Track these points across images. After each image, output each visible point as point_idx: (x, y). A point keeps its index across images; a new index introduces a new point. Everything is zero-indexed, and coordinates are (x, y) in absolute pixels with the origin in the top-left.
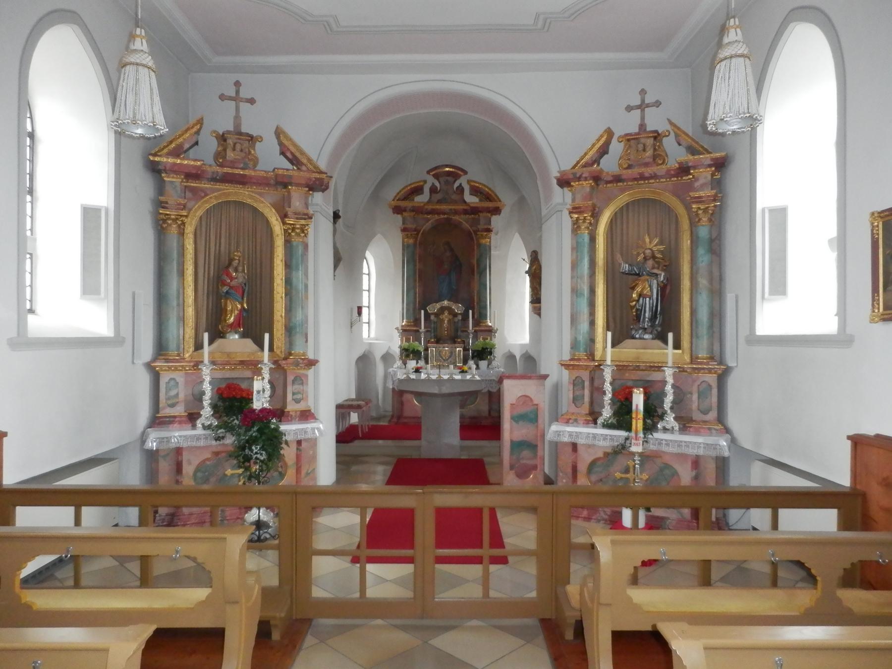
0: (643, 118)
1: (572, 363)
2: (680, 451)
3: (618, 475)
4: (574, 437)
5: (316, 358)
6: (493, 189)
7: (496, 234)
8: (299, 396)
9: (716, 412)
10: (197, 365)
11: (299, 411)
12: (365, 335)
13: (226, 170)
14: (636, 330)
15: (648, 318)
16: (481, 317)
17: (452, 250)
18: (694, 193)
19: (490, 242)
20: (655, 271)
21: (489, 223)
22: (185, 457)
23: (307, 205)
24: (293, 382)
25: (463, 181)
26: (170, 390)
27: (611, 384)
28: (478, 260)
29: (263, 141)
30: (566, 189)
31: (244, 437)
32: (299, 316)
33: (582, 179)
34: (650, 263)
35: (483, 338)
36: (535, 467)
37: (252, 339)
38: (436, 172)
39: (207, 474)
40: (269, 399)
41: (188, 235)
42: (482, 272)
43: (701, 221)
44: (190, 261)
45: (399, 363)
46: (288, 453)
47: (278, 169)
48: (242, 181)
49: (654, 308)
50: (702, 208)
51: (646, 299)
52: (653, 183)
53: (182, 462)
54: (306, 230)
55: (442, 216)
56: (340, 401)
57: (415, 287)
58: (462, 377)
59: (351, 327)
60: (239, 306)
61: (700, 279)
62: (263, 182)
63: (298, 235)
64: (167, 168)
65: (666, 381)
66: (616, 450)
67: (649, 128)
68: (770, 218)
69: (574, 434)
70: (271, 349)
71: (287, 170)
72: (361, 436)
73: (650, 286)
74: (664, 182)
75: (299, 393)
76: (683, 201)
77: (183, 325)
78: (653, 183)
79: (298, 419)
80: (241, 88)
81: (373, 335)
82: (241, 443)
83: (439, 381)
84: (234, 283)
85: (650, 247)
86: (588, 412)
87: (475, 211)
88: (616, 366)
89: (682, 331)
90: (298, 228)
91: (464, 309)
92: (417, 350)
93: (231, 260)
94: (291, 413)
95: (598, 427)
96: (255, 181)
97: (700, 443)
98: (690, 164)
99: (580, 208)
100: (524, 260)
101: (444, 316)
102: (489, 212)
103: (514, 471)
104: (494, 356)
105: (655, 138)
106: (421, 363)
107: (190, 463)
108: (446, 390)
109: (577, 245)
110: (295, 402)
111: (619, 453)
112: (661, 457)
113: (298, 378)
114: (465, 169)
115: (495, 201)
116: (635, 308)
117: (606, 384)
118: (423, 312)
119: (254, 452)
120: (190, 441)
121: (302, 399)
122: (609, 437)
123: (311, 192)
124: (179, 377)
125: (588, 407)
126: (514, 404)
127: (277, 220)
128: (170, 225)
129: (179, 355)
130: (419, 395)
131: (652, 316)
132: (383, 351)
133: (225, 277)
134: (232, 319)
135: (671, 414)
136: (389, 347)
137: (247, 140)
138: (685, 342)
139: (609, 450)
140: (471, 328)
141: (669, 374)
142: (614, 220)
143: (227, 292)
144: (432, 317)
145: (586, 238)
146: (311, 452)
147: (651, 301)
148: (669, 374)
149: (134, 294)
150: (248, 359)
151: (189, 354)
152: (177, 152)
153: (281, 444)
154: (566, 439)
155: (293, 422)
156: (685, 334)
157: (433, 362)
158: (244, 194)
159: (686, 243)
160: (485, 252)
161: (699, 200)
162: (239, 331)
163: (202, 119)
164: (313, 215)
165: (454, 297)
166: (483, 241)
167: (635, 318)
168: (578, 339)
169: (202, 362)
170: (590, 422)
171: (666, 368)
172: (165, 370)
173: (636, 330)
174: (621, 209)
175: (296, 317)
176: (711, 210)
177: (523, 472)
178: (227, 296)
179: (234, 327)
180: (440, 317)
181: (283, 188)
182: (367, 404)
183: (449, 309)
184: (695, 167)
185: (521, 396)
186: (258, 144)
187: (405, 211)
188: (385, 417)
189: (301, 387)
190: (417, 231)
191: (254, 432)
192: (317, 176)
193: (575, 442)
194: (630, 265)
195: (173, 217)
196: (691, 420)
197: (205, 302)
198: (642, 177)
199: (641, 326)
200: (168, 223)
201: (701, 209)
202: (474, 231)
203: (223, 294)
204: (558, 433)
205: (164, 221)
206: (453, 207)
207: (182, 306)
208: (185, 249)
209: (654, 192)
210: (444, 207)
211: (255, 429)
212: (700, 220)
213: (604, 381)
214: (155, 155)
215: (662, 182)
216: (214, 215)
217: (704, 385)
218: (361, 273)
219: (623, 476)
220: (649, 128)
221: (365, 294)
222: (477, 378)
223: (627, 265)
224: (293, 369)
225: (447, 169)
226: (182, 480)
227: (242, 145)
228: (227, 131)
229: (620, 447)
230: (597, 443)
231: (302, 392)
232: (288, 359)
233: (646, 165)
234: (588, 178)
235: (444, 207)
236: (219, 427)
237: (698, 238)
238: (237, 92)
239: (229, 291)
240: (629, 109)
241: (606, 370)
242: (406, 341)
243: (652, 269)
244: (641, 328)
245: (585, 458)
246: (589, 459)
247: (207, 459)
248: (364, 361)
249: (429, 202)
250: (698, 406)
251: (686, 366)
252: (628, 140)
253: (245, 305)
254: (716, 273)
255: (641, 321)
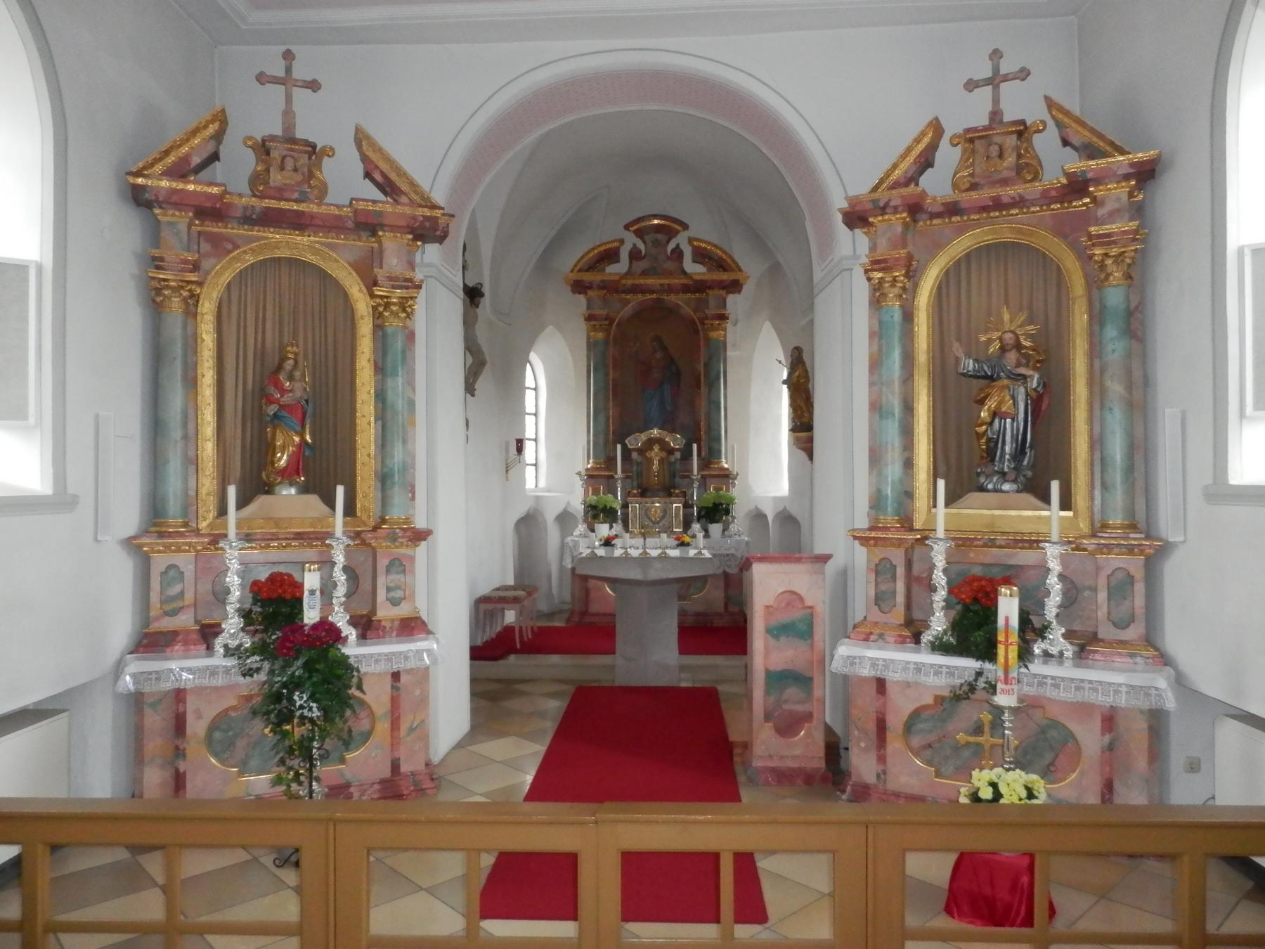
0: (996, 100)
1: (873, 534)
2: (1080, 699)
3: (962, 737)
4: (880, 667)
5: (430, 528)
6: (728, 250)
7: (735, 324)
8: (399, 594)
9: (1144, 624)
10: (217, 538)
11: (397, 619)
12: (530, 483)
13: (268, 203)
14: (987, 477)
15: (1010, 455)
16: (711, 455)
17: (665, 349)
18: (1097, 228)
19: (725, 336)
20: (1022, 371)
21: (724, 305)
22: (191, 705)
23: (412, 265)
24: (388, 571)
25: (681, 240)
26: (169, 585)
27: (945, 571)
28: (706, 365)
29: (336, 154)
30: (857, 231)
31: (279, 679)
32: (398, 455)
33: (888, 210)
34: (1012, 357)
35: (715, 488)
36: (808, 717)
37: (318, 495)
38: (638, 227)
39: (230, 733)
40: (344, 599)
41: (205, 316)
42: (713, 384)
43: (1111, 278)
44: (208, 361)
45: (581, 528)
46: (375, 695)
47: (357, 200)
48: (299, 223)
49: (1020, 437)
50: (1112, 254)
51: (1005, 420)
52: (1017, 214)
53: (184, 713)
54: (410, 306)
55: (649, 296)
56: (485, 589)
57: (606, 409)
58: (681, 552)
59: (507, 471)
60: (297, 439)
61: (1108, 383)
62: (333, 225)
63: (395, 314)
64: (161, 199)
65: (1049, 569)
66: (958, 692)
67: (1008, 117)
68: (1254, 265)
69: (881, 663)
70: (350, 510)
71: (374, 202)
72: (518, 647)
73: (1013, 398)
74: (1038, 212)
75: (398, 588)
76: (1074, 246)
77: (195, 471)
78: (1017, 214)
79: (394, 633)
80: (293, 62)
81: (542, 484)
82: (274, 689)
83: (644, 560)
84: (286, 399)
85: (1012, 329)
86: (902, 622)
87: (700, 287)
88: (954, 539)
89: (1073, 476)
90: (394, 304)
91: (684, 441)
92: (611, 508)
93: (283, 359)
94: (383, 623)
95: (923, 649)
96: (320, 223)
97: (1120, 685)
98: (1090, 175)
99: (885, 261)
100: (780, 362)
101: (653, 454)
102: (723, 288)
103: (771, 724)
104: (732, 516)
105: (1020, 134)
106: (618, 528)
107: (199, 716)
108: (655, 574)
109: (881, 328)
110: (392, 604)
111: (965, 699)
112: (1042, 707)
113: (396, 562)
114: (686, 222)
115: (732, 270)
116: (985, 438)
117: (935, 572)
118: (619, 446)
119: (298, 704)
120: (199, 678)
121: (405, 598)
122: (944, 670)
123: (419, 243)
124: (185, 561)
125: (903, 613)
126: (771, 607)
127: (360, 291)
128: (169, 298)
129: (186, 525)
130: (612, 581)
131: (1016, 449)
132: (559, 510)
133: (272, 390)
134: (283, 463)
135: (1058, 627)
136: (568, 502)
137: (306, 152)
138: (1080, 498)
139: (946, 693)
140: (695, 472)
141: (1053, 555)
142: (943, 286)
143: (275, 415)
144: (635, 455)
145: (897, 316)
146: (418, 692)
147: (1015, 424)
148: (1053, 555)
149: (97, 416)
150: (312, 530)
151: (208, 522)
152: (181, 171)
153: (350, 687)
154: (866, 671)
155: (388, 639)
156: (1079, 483)
157: (634, 527)
158: (301, 245)
159: (1080, 320)
160: (717, 352)
161: (1107, 240)
162: (297, 482)
163: (223, 111)
164: (422, 281)
165: (669, 424)
166: (714, 334)
167: (985, 455)
168: (884, 493)
169: (225, 536)
170: (908, 640)
171: (1047, 544)
172: (159, 552)
173: (987, 477)
174: (958, 264)
175: (393, 457)
176: (1130, 258)
177: (788, 726)
178: (276, 422)
179: (288, 475)
180: (647, 454)
181: (371, 236)
182: (530, 594)
183: (660, 441)
184: (1098, 181)
185: (784, 592)
186: (326, 161)
187: (590, 287)
188: (561, 612)
189: (401, 577)
190: (610, 319)
191: (297, 669)
192: (428, 213)
193: (882, 677)
194: (976, 361)
195: (173, 284)
196: (1094, 638)
197: (239, 431)
198: (998, 205)
199: (996, 468)
200: (165, 296)
201: (1110, 257)
202: (699, 318)
203: (268, 419)
204: (851, 660)
205: (158, 291)
206: (666, 281)
207: (191, 438)
208: (199, 340)
209: (1020, 231)
210: (651, 281)
211: (300, 663)
212: (1108, 275)
213: (932, 567)
214: (138, 174)
215: (1033, 212)
216: (252, 285)
217: (1120, 575)
218: (522, 389)
219: (971, 739)
220: (1008, 117)
221: (529, 421)
222: (706, 554)
223: (971, 361)
224: (387, 547)
225: (656, 222)
226: (185, 745)
227: (296, 160)
228: (271, 136)
229: (965, 688)
230: (923, 679)
231: (403, 587)
232: (378, 530)
233: (1005, 182)
234: (900, 209)
235: (651, 281)
236: (253, 651)
237: (1103, 308)
238: (288, 70)
239: (279, 414)
240: (971, 85)
241: (935, 547)
242: (593, 494)
243: (1016, 367)
244: (997, 472)
245: (901, 707)
246: (908, 708)
247: (233, 708)
248: (528, 524)
249: (629, 273)
250: (1109, 613)
251: (1085, 541)
252: (971, 141)
253: (308, 438)
254: (1137, 374)
255: (997, 459)
